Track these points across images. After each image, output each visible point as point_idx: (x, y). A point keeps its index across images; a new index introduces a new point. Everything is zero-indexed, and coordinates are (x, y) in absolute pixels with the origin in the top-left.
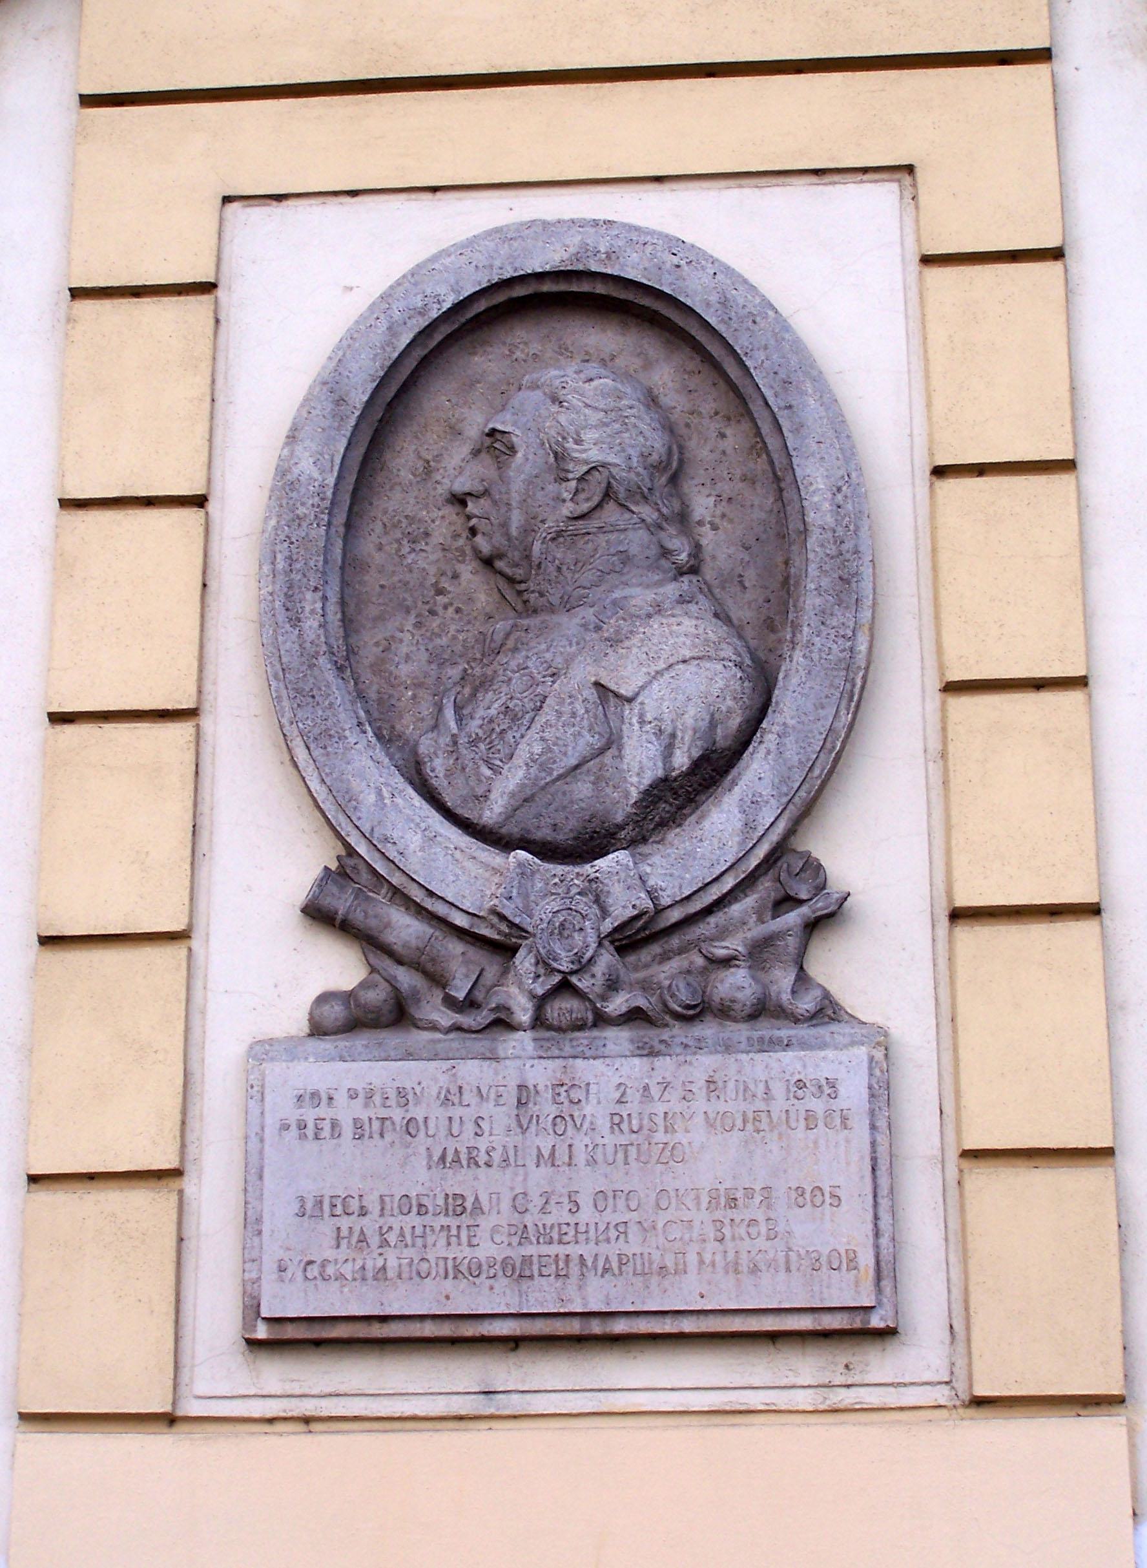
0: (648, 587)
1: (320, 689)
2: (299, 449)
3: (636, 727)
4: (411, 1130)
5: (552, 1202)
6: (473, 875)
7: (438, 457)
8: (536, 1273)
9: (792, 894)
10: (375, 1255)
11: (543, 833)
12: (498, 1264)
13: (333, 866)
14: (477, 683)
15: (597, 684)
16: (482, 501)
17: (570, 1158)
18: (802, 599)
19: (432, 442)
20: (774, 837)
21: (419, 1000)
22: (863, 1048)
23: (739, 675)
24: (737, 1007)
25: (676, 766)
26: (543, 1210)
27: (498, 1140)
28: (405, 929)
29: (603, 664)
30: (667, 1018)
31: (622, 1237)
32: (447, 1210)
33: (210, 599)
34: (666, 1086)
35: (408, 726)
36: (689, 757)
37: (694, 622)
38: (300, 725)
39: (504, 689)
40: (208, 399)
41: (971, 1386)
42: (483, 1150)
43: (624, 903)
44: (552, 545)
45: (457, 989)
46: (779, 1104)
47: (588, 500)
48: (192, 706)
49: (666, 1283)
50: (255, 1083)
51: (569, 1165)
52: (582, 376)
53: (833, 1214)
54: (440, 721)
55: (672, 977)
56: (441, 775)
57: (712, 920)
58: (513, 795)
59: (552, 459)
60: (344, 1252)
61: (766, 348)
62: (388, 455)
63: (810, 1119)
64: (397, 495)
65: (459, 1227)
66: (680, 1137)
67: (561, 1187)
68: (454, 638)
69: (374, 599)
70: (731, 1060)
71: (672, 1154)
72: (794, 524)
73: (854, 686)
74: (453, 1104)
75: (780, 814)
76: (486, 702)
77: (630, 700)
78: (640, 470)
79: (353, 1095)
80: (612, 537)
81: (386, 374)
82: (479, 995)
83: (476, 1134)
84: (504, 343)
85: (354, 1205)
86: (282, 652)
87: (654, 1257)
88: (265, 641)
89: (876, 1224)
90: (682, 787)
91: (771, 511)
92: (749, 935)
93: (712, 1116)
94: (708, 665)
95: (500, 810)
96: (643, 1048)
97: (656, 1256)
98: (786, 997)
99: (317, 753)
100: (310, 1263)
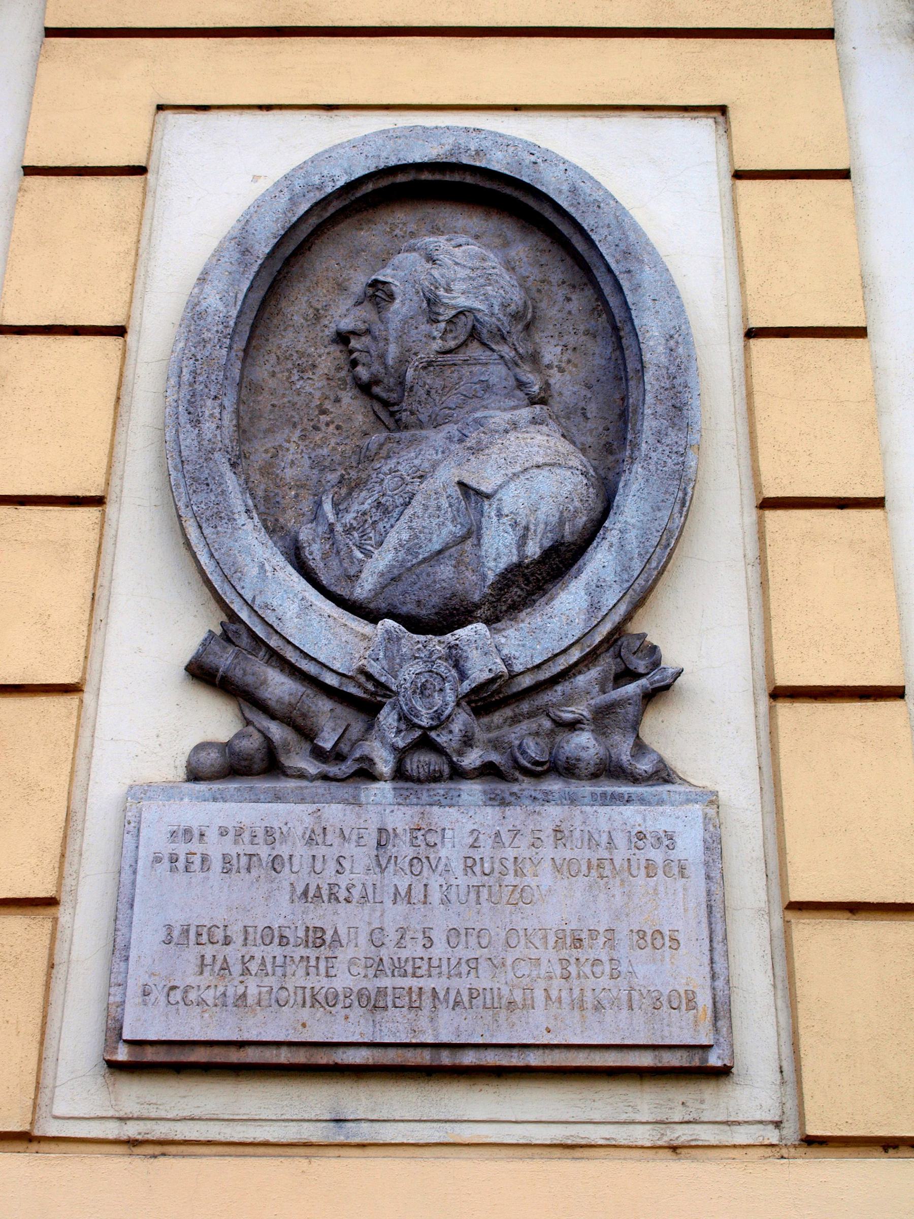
0: (505, 410)
1: (214, 478)
2: (207, 288)
3: (495, 519)
4: (276, 867)
5: (407, 937)
6: (343, 640)
7: (326, 307)
8: (390, 1004)
9: (632, 667)
10: (236, 983)
11: (409, 608)
12: (355, 994)
13: (218, 631)
14: (353, 484)
15: (461, 484)
16: (363, 338)
17: (425, 896)
18: (639, 423)
19: (321, 295)
20: (616, 618)
21: (289, 751)
22: (697, 806)
23: (585, 481)
24: (582, 765)
25: (529, 554)
26: (399, 945)
27: (358, 877)
28: (278, 686)
29: (466, 468)
30: (517, 774)
31: (473, 972)
32: (307, 941)
33: (122, 410)
34: (515, 833)
35: (289, 519)
36: (541, 547)
37: (546, 438)
38: (195, 508)
39: (377, 488)
40: (133, 253)
41: (802, 1124)
42: (343, 887)
43: (480, 669)
44: (424, 373)
45: (325, 741)
46: (621, 853)
47: (455, 338)
48: (98, 493)
49: (514, 1018)
50: (132, 819)
51: (425, 903)
52: (453, 242)
53: (672, 957)
54: (320, 513)
55: (522, 738)
56: (318, 558)
57: (559, 688)
58: (382, 574)
59: (425, 305)
60: (207, 978)
61: (609, 226)
62: (283, 304)
63: (650, 869)
64: (290, 334)
65: (318, 958)
66: (529, 880)
67: (416, 924)
68: (334, 449)
69: (266, 415)
70: (576, 811)
71: (521, 897)
72: (631, 365)
73: (686, 494)
74: (317, 844)
75: (622, 597)
76: (361, 499)
77: (488, 497)
78: (501, 316)
79: (223, 832)
80: (476, 369)
81: (286, 233)
82: (344, 748)
83: (337, 871)
84: (386, 223)
85: (219, 935)
86: (182, 447)
87: (503, 992)
88: (168, 439)
89: (712, 967)
90: (533, 575)
91: (610, 358)
92: (593, 702)
93: (558, 862)
94: (558, 471)
95: (370, 587)
96: (494, 799)
97: (505, 991)
98: (625, 758)
99: (207, 531)
100: (173, 988)
